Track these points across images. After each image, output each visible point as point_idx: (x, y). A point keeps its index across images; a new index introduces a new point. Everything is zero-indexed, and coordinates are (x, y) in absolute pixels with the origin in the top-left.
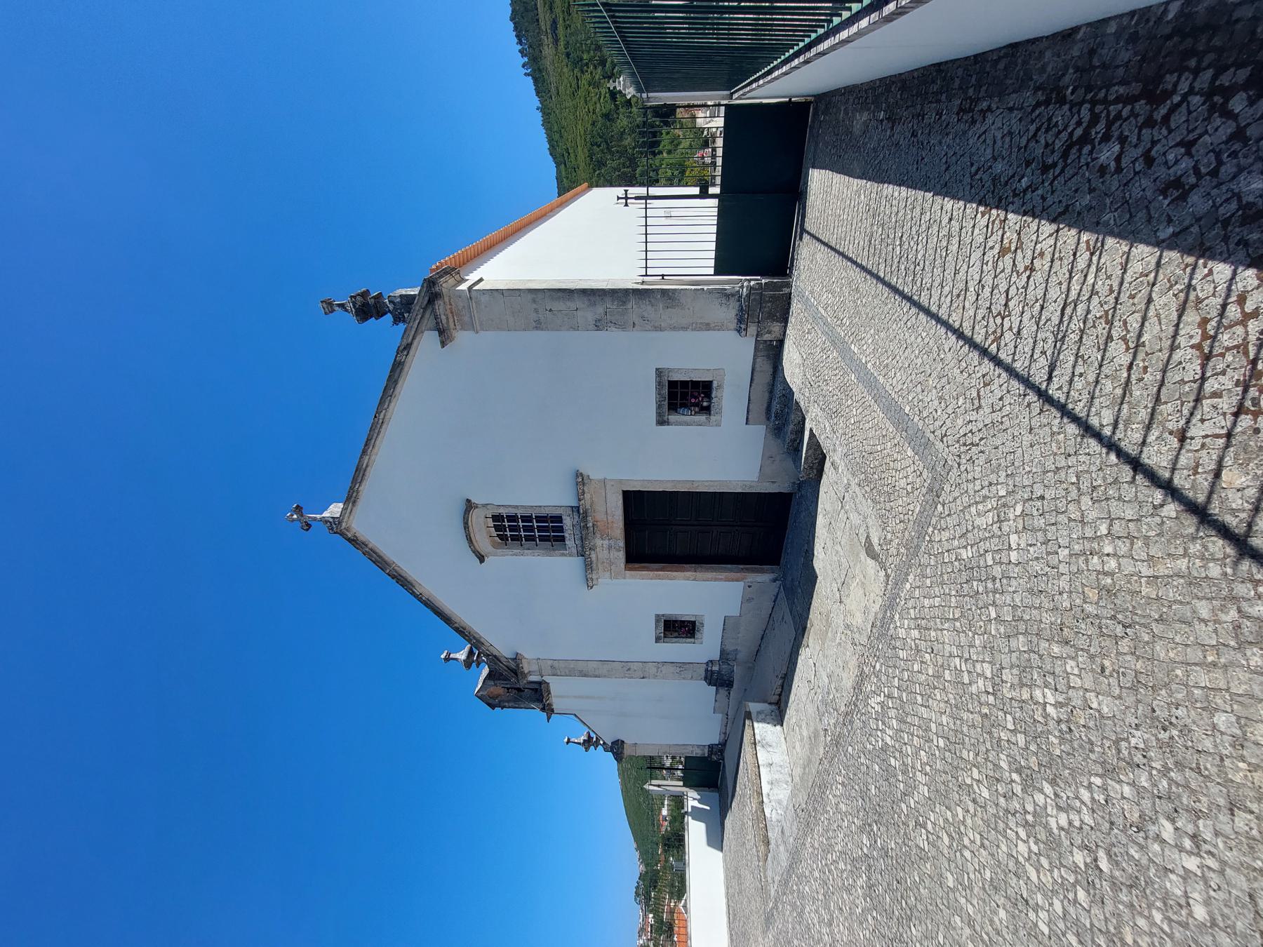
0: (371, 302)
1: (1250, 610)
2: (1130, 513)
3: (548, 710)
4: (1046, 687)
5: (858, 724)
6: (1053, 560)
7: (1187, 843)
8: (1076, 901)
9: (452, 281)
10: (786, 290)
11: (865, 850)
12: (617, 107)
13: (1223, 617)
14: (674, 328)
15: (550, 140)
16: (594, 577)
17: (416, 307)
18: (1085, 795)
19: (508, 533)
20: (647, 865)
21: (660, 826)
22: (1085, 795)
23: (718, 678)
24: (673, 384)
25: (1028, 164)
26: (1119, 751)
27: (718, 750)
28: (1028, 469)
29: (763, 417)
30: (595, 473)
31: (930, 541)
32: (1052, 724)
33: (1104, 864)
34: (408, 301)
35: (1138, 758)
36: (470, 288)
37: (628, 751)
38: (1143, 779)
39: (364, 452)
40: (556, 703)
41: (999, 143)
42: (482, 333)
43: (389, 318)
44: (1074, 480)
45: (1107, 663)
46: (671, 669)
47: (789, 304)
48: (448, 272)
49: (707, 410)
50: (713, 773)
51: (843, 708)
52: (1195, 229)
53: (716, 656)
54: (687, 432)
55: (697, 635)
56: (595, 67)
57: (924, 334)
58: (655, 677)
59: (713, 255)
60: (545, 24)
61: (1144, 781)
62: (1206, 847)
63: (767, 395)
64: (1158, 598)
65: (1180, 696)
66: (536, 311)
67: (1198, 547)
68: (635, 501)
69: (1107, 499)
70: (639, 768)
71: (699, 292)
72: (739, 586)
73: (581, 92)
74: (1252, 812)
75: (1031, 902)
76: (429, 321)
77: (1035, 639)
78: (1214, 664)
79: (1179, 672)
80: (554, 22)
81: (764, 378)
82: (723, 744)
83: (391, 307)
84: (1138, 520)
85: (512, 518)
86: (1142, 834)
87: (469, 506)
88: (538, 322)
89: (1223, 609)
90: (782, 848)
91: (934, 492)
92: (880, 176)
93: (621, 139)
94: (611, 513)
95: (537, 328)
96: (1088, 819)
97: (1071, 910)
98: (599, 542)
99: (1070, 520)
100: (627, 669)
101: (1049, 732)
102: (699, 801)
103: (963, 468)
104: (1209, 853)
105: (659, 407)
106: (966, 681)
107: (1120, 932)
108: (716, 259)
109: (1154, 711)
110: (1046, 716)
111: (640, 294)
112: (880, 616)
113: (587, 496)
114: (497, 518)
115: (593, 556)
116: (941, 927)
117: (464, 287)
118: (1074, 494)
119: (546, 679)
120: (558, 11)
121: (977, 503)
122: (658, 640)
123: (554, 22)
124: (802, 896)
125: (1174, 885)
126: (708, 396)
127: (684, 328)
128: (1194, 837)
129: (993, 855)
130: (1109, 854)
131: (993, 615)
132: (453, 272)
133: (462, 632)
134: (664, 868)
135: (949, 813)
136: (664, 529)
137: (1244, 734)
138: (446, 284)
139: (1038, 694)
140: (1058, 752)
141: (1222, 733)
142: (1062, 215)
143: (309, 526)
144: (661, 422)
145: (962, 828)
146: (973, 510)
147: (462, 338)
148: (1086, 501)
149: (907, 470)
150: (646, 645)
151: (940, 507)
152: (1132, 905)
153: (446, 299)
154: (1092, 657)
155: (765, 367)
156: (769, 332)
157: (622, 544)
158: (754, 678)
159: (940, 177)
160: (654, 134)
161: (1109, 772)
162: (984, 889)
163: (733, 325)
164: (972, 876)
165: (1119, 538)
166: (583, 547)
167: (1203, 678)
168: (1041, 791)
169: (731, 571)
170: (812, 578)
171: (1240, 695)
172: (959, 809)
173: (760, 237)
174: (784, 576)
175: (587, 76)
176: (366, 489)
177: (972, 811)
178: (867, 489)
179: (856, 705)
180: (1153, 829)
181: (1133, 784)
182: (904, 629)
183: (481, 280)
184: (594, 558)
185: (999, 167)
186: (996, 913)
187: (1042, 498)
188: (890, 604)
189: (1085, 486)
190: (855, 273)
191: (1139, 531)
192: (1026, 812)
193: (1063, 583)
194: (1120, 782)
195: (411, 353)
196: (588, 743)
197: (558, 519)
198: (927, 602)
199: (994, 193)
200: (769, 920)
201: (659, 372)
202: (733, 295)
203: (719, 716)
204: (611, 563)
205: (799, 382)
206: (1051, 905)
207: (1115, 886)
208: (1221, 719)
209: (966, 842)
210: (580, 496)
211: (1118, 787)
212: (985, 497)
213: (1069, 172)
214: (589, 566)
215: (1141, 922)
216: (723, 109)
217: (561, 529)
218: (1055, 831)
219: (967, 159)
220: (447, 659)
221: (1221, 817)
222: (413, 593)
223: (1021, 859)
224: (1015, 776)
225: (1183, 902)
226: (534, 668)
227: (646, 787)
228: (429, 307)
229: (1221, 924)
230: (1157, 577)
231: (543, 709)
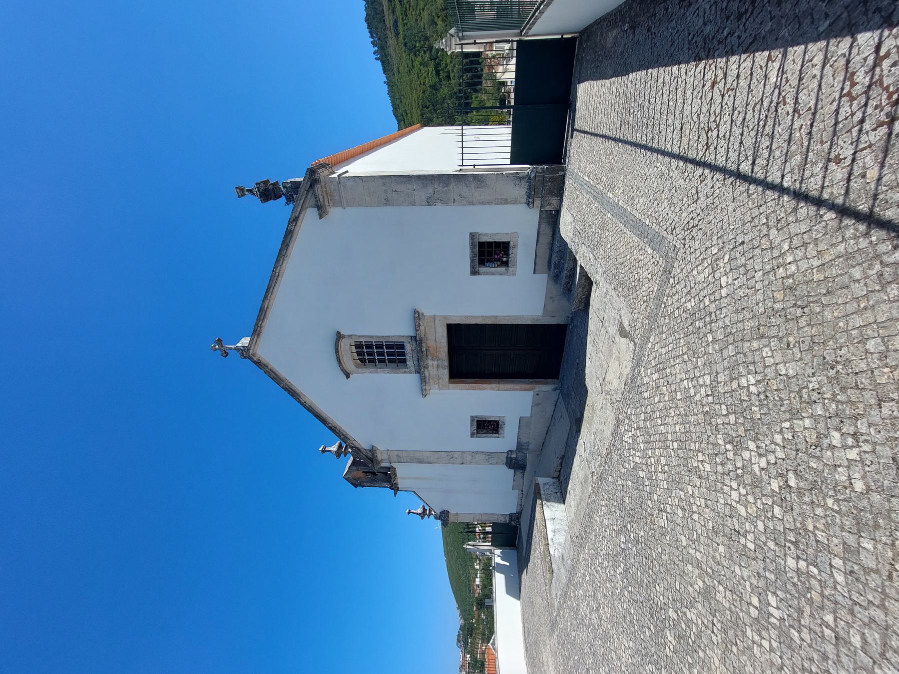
0: (271, 187)
1: (889, 259)
2: (804, 227)
3: (395, 488)
4: (749, 374)
5: (616, 457)
6: (752, 283)
7: (850, 441)
8: (773, 516)
9: (326, 172)
10: (561, 173)
11: (622, 546)
12: (440, 80)
13: (870, 272)
14: (483, 203)
15: (394, 105)
16: (427, 388)
17: (302, 190)
18: (778, 438)
19: (367, 357)
20: (465, 620)
21: (474, 590)
22: (778, 438)
23: (515, 463)
24: (482, 245)
25: (728, 18)
26: (801, 397)
27: (516, 517)
28: (732, 227)
29: (546, 267)
30: (427, 311)
31: (665, 307)
32: (753, 398)
33: (792, 482)
34: (296, 186)
35: (815, 396)
36: (339, 176)
37: (452, 519)
38: (818, 409)
39: (265, 297)
40: (401, 483)
41: (708, 12)
42: (348, 209)
43: (283, 199)
44: (765, 221)
45: (791, 339)
46: (482, 457)
47: (564, 183)
48: (323, 166)
49: (506, 264)
50: (514, 536)
51: (605, 452)
52: (845, 15)
53: (514, 447)
54: (492, 281)
55: (500, 431)
56: (425, 52)
57: (658, 165)
58: (471, 463)
59: (509, 149)
60: (389, 23)
61: (819, 411)
62: (862, 438)
63: (548, 251)
64: (826, 278)
65: (842, 341)
66: (386, 191)
67: (852, 231)
68: (454, 331)
69: (788, 225)
70: (458, 532)
71: (499, 176)
72: (531, 393)
73: (415, 70)
74: (893, 400)
75: (741, 531)
76: (311, 200)
77: (740, 344)
78: (865, 308)
79: (841, 324)
80: (396, 22)
81: (546, 239)
82: (520, 513)
83: (284, 190)
84: (810, 230)
85: (369, 346)
86: (819, 449)
87: (339, 336)
88: (387, 199)
89: (870, 267)
90: (562, 570)
91: (667, 272)
92: (623, 70)
93: (443, 102)
94: (439, 340)
95: (386, 204)
96: (781, 455)
97: (770, 525)
98: (430, 363)
99: (763, 250)
100: (451, 457)
101: (752, 405)
102: (502, 559)
103: (687, 246)
104: (866, 441)
105: (472, 261)
106: (692, 393)
107: (804, 525)
108: (512, 140)
109: (825, 358)
110: (749, 394)
111: (458, 178)
112: (630, 376)
113: (422, 328)
114: (358, 346)
115: (426, 372)
116: (678, 578)
117: (335, 175)
118: (765, 230)
119: (394, 465)
120: (398, 13)
121: (697, 266)
122: (472, 435)
123: (396, 22)
124: (577, 598)
125: (841, 476)
126: (507, 253)
127: (490, 203)
128: (855, 435)
129: (713, 510)
130: (796, 473)
131: (710, 339)
132: (329, 166)
133: (334, 430)
134: (477, 622)
135: (682, 493)
136: (476, 352)
137: (887, 347)
138: (322, 173)
139: (743, 382)
140: (758, 416)
141: (872, 354)
142: (750, 46)
143: (227, 354)
144: (474, 272)
145: (692, 501)
146: (695, 272)
147: (334, 212)
148: (774, 232)
149: (648, 263)
150: (464, 439)
151: (671, 281)
152: (813, 502)
153: (323, 184)
154: (780, 339)
155: (547, 230)
156: (550, 204)
157: (446, 363)
158: (544, 465)
159: (667, 51)
160: (467, 98)
161: (794, 414)
162: (708, 537)
163: (524, 200)
164: (699, 531)
165: (797, 248)
166: (419, 366)
167: (858, 321)
168: (747, 449)
169: (524, 383)
170: (583, 392)
171: (883, 322)
172: (689, 487)
173: (543, 139)
174: (562, 385)
175: (419, 59)
176: (268, 326)
177: (698, 484)
178: (620, 289)
179: (614, 445)
180: (826, 442)
181: (811, 416)
182: (648, 377)
183: (347, 172)
184: (427, 374)
185: (708, 29)
186: (716, 550)
187: (743, 243)
188: (638, 363)
189: (772, 221)
190: (609, 144)
191: (811, 237)
192: (737, 468)
193: (759, 297)
194: (802, 418)
195: (298, 223)
196: (423, 515)
197: (402, 346)
198: (663, 351)
199: (703, 49)
200: (553, 625)
201: (472, 236)
202: (524, 178)
203: (517, 492)
204: (439, 379)
205: (570, 234)
206: (755, 527)
207: (800, 494)
208: (871, 345)
209: (695, 508)
210: (417, 328)
211: (801, 422)
212: (703, 259)
213: (757, 11)
214: (423, 380)
215: (819, 511)
216: (515, 43)
217: (403, 354)
218: (758, 473)
219: (686, 32)
220: (324, 451)
221: (872, 412)
222: (300, 402)
223: (734, 504)
224: (729, 447)
225: (847, 484)
226: (385, 457)
227: (465, 546)
228: (308, 191)
229: (874, 488)
230: (824, 265)
231: (391, 488)
